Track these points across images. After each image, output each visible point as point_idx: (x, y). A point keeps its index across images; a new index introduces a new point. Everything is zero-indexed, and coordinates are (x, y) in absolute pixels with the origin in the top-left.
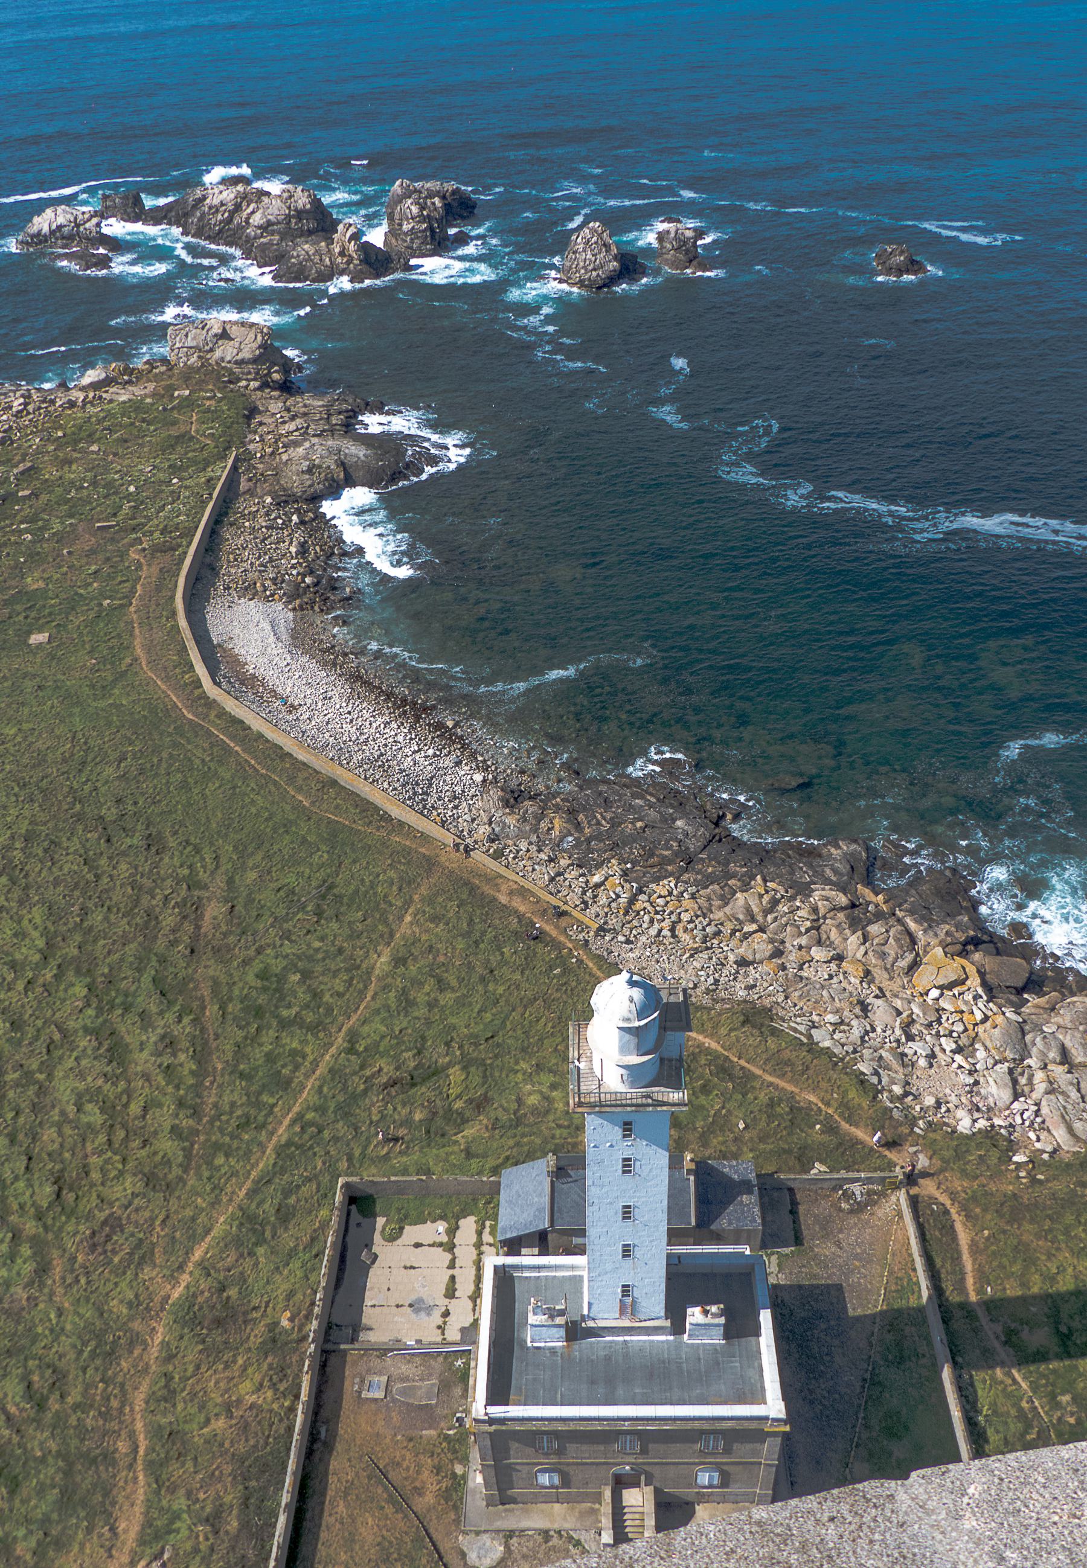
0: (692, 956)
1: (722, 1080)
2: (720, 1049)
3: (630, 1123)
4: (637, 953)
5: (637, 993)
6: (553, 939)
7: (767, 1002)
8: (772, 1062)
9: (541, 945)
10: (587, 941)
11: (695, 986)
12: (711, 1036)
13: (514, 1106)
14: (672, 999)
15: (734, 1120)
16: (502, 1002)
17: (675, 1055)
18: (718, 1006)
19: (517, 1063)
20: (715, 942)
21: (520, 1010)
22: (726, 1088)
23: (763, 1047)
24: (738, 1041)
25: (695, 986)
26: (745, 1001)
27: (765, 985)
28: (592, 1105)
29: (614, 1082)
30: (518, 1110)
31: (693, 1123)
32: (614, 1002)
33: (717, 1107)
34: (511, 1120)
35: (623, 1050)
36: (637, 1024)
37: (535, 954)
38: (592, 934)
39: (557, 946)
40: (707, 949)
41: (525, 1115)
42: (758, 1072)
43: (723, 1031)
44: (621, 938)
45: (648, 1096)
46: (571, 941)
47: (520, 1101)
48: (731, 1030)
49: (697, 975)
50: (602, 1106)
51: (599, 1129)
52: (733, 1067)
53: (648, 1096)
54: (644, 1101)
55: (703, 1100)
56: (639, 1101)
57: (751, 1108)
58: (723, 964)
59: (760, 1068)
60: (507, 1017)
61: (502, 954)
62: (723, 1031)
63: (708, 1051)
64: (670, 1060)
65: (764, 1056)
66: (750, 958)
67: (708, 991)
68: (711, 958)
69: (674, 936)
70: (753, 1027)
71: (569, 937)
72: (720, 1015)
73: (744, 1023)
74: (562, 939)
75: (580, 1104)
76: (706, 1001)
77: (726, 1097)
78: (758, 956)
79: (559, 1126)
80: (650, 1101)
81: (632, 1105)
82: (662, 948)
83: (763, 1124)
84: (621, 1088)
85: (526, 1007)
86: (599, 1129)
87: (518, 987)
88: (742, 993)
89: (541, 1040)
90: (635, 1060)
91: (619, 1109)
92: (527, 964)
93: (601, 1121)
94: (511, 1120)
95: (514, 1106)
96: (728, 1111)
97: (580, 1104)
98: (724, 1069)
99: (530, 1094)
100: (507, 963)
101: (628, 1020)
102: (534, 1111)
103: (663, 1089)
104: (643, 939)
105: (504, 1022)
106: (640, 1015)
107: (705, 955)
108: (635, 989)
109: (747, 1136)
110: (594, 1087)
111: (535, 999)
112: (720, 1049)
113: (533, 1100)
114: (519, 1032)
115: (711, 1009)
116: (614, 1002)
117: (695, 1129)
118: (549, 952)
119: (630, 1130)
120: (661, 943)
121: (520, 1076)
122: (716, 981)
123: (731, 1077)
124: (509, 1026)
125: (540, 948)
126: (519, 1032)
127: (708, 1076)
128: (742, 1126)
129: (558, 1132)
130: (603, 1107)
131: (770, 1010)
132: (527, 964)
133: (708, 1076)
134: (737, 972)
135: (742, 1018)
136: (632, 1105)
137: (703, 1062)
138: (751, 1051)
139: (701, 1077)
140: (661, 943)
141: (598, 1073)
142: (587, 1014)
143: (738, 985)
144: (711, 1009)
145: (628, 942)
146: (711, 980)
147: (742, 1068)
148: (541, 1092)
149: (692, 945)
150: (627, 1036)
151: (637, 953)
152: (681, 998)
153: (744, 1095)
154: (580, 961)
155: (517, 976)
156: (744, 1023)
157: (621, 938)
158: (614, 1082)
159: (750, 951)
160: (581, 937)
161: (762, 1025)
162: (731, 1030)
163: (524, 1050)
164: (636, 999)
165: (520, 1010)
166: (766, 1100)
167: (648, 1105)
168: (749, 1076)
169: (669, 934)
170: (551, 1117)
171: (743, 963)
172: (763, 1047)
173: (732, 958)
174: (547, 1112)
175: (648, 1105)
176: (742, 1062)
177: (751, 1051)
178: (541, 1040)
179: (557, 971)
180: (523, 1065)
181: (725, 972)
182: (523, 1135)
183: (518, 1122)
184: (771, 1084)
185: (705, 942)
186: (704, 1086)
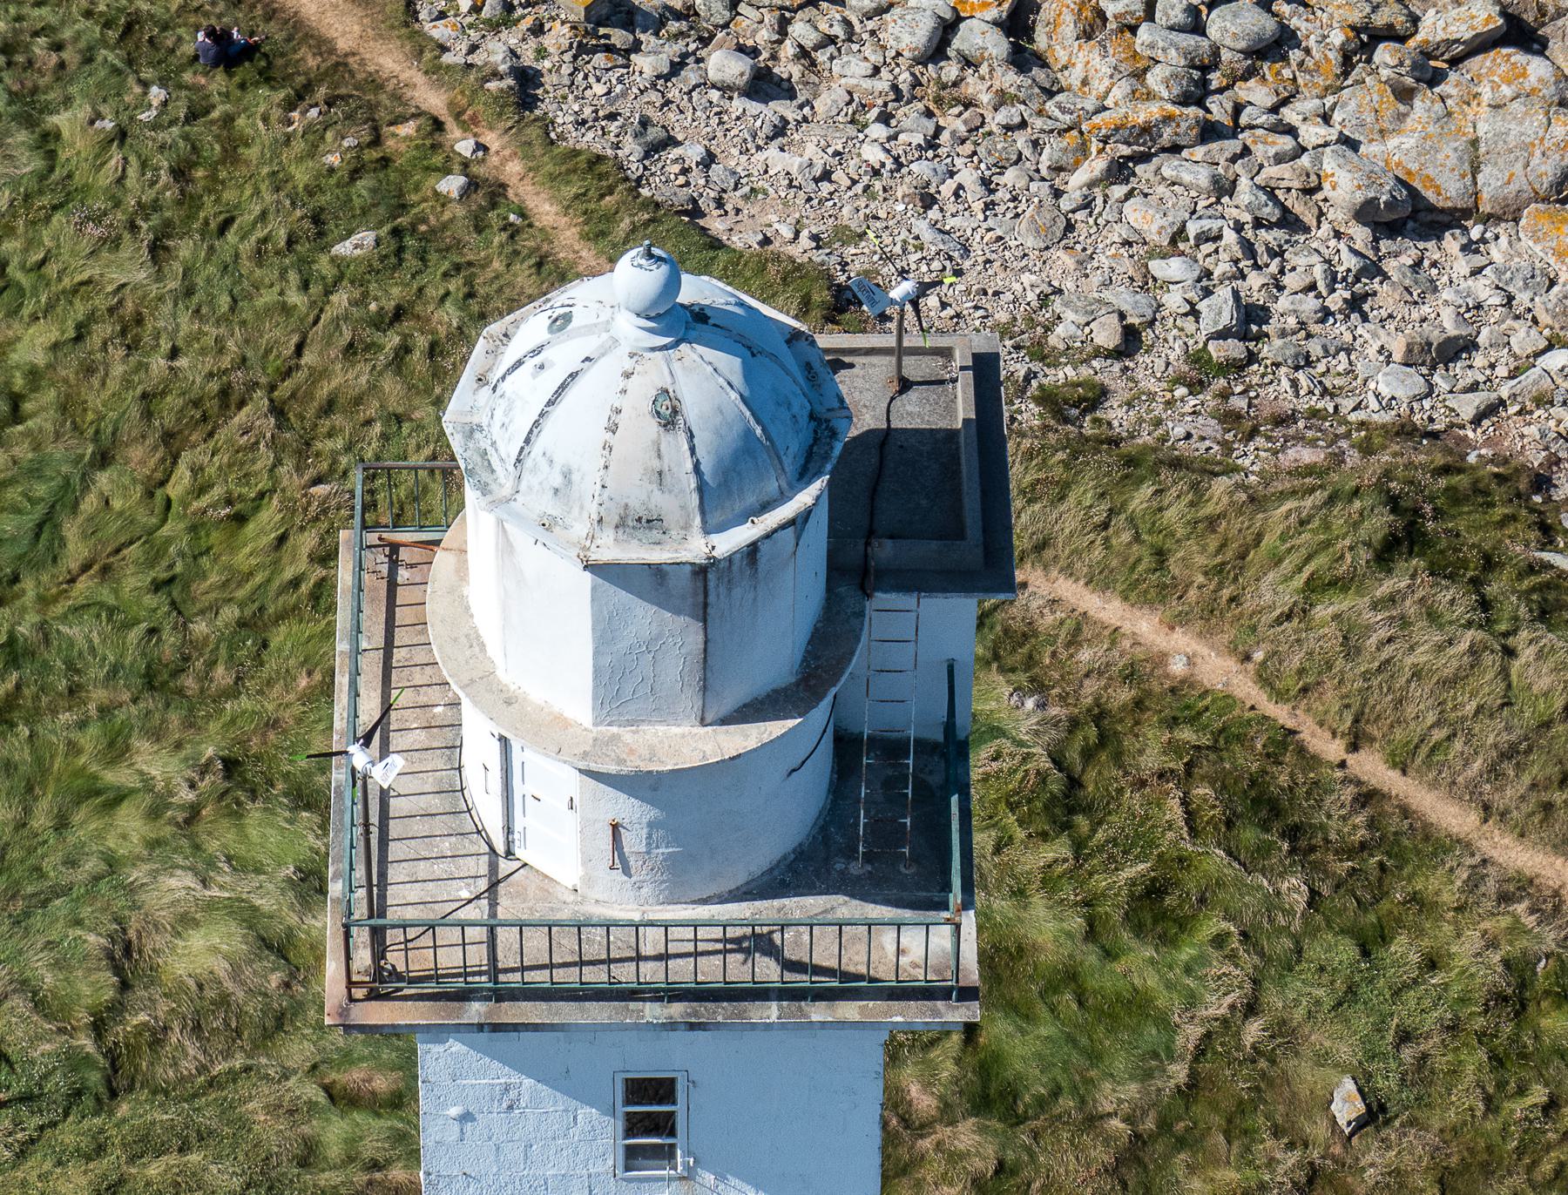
0: (1119, 171)
1: (1254, 860)
2: (1246, 689)
3: (662, 1089)
4: (809, 151)
5: (707, 380)
6: (339, 67)
7: (1526, 439)
8: (1539, 768)
9: (267, 99)
10: (526, 81)
11: (1131, 341)
12: (1209, 616)
13: (95, 987)
14: (914, 413)
15: (1306, 1075)
16: (41, 410)
17: (917, 716)
18: (1252, 458)
19: (117, 750)
20: (1257, 94)
21: (140, 457)
22: (1273, 903)
23: (1487, 684)
24: (1351, 650)
25: (1131, 341)
26: (1406, 431)
27: (1524, 339)
28: (451, 992)
29: (566, 854)
30: (117, 1009)
31: (1083, 1091)
32: (576, 408)
33: (1217, 1006)
34: (74, 1061)
35: (617, 688)
36: (696, 547)
37: (232, 148)
38: (558, 36)
39: (354, 97)
40: (1209, 132)
41: (156, 1037)
42: (1451, 816)
43: (1273, 591)
44: (723, 64)
45: (761, 943)
46: (435, 71)
47: (126, 961)
48: (1316, 587)
49: (1146, 282)
50: (501, 995)
51: (492, 1120)
52: (1318, 788)
53: (761, 943)
54: (738, 970)
55: (1138, 966)
56: (710, 971)
57: (1404, 1012)
58: (1289, 222)
59: (1472, 795)
60: (66, 498)
61: (48, 142)
62: (1273, 591)
63: (1183, 703)
64: (892, 748)
65: (1493, 734)
66: (1447, 189)
67: (1199, 372)
68: (1223, 188)
69: (1023, 58)
70: (1442, 570)
71: (427, 52)
72: (1256, 501)
73: (1386, 554)
74: (389, 60)
75: (382, 984)
76: (1190, 424)
77: (1268, 955)
78: (1492, 183)
79: (342, 1099)
80: (768, 970)
81: (672, 994)
82: (953, 122)
83: (1463, 1100)
84: (619, 900)
85: (172, 442)
86: (492, 1120)
87: (131, 331)
88: (1393, 385)
89: (254, 625)
90: (687, 742)
91: (598, 1013)
92: (189, 202)
93: (501, 1074)
94: (74, 1061)
95: (95, 987)
96: (1282, 1029)
97: (382, 984)
98: (1266, 803)
99: (186, 921)
100: (69, 195)
101: (650, 523)
102: (209, 1013)
103: (845, 907)
104: (850, 70)
105: (47, 525)
106: (718, 496)
107: (1193, 170)
108: (691, 353)
109: (1374, 1159)
110: (461, 889)
111: (228, 400)
112: (1246, 689)
113: (201, 954)
114: (133, 581)
115: (1210, 470)
116: (576, 408)
117: (1092, 1121)
118: (315, 136)
119: (664, 1125)
120: (953, 97)
121: (130, 824)
122: (1251, 319)
123: (1302, 842)
124: (76, 550)
125: (260, 113)
126: (133, 581)
127: (1173, 836)
128: (1346, 1106)
129: (334, 1132)
130: (498, 998)
131: (1542, 482)
132: (189, 202)
133: (1173, 836)
134: (1373, 269)
135: (1380, 523)
136: (672, 994)
137: (1151, 760)
138: (1421, 709)
139: (1138, 841)
140: (953, 97)
141: (490, 814)
142: (417, 494)
143: (1370, 337)
144: (1210, 470)
145: (763, 85)
146: (1219, 310)
147: (1368, 797)
148: (248, 915)
149: (1124, 108)
150: (644, 617)
151: (809, 151)
152: (962, 407)
153: (1369, 943)
154: (487, 193)
155: (129, 269)
156: (1386, 554)
157: (723, 64)
158: (566, 854)
159: (1450, 154)
160: (495, 52)
161: (1490, 563)
162: (1316, 587)
163: (155, 680)
164: (694, 408)
165: (140, 457)
166: (1490, 973)
167: (760, 994)
168: (1397, 843)
169: (997, 45)
170: (298, 1050)
171: (1408, 216)
172: (1487, 684)
173: (1344, 186)
174: (279, 1023)
175: (760, 994)
176: (1371, 767)
177: (1421, 709)
178: (254, 625)
179: (357, 244)
180: (154, 763)
181: (1305, 263)
182: (144, 1145)
183: (118, 1076)
184: (1518, 888)
185: (1196, 95)
186: (1152, 893)
